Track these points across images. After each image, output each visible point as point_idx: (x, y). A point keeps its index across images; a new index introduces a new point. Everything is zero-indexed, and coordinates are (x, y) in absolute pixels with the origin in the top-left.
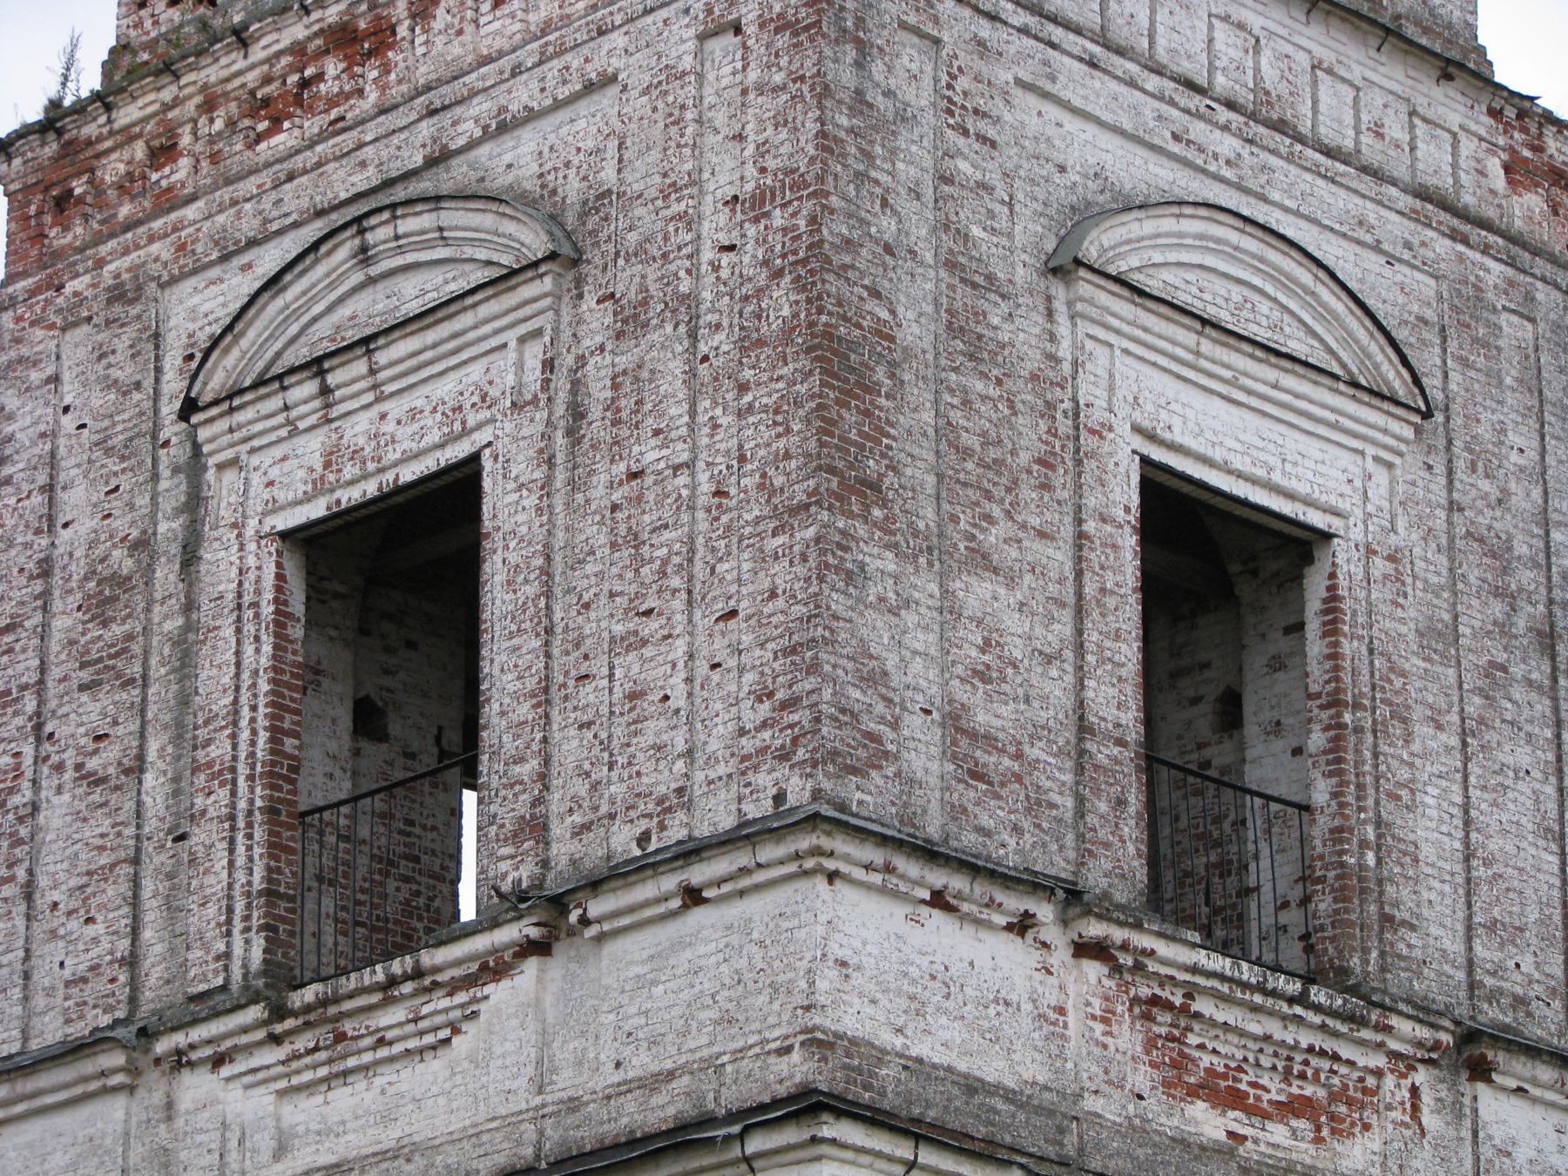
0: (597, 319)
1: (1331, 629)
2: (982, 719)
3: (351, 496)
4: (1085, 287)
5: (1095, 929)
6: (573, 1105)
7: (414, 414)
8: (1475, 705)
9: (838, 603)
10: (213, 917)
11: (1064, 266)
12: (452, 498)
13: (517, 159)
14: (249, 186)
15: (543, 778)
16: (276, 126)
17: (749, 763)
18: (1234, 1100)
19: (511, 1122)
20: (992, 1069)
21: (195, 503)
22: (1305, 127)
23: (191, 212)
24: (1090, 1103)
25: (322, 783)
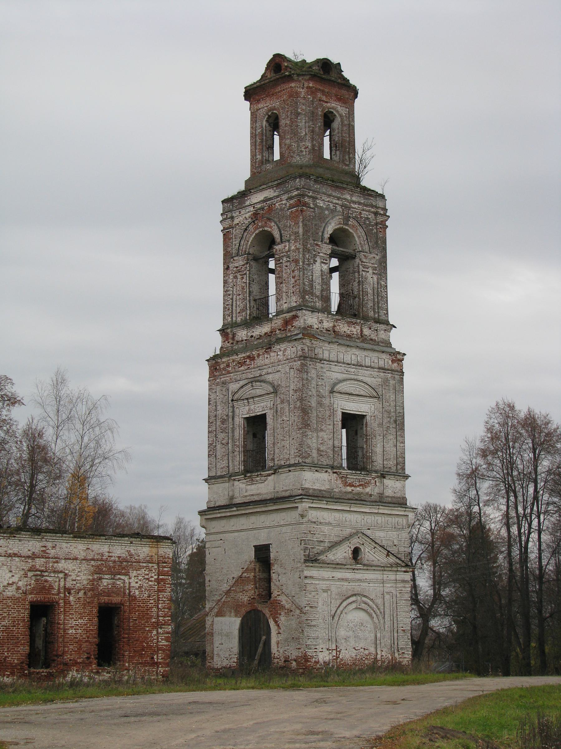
0: (279, 401)
1: (366, 427)
2: (322, 449)
3: (252, 415)
4: (335, 394)
5: (335, 471)
6: (278, 492)
7: (259, 407)
8: (385, 432)
9: (305, 439)
10: (237, 464)
11: (332, 392)
12: (263, 417)
13: (270, 378)
14: (238, 373)
15: (274, 454)
16: (242, 366)
17: (296, 456)
18: (353, 486)
19: (271, 493)
20: (323, 488)
21: (233, 412)
22: (364, 365)
23: (232, 375)
24: (335, 490)
25: (250, 447)
